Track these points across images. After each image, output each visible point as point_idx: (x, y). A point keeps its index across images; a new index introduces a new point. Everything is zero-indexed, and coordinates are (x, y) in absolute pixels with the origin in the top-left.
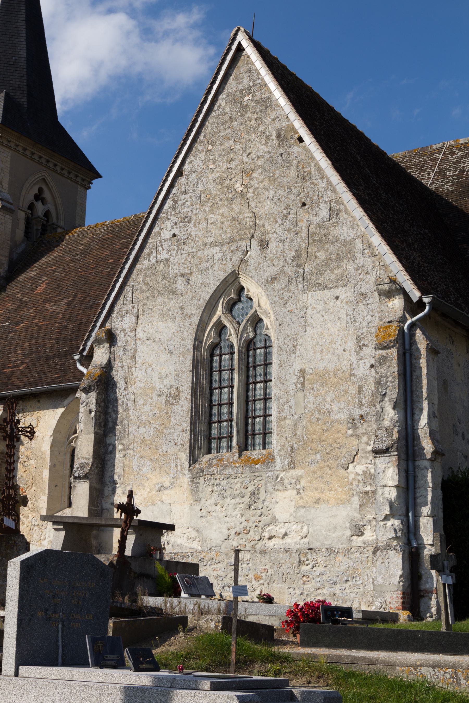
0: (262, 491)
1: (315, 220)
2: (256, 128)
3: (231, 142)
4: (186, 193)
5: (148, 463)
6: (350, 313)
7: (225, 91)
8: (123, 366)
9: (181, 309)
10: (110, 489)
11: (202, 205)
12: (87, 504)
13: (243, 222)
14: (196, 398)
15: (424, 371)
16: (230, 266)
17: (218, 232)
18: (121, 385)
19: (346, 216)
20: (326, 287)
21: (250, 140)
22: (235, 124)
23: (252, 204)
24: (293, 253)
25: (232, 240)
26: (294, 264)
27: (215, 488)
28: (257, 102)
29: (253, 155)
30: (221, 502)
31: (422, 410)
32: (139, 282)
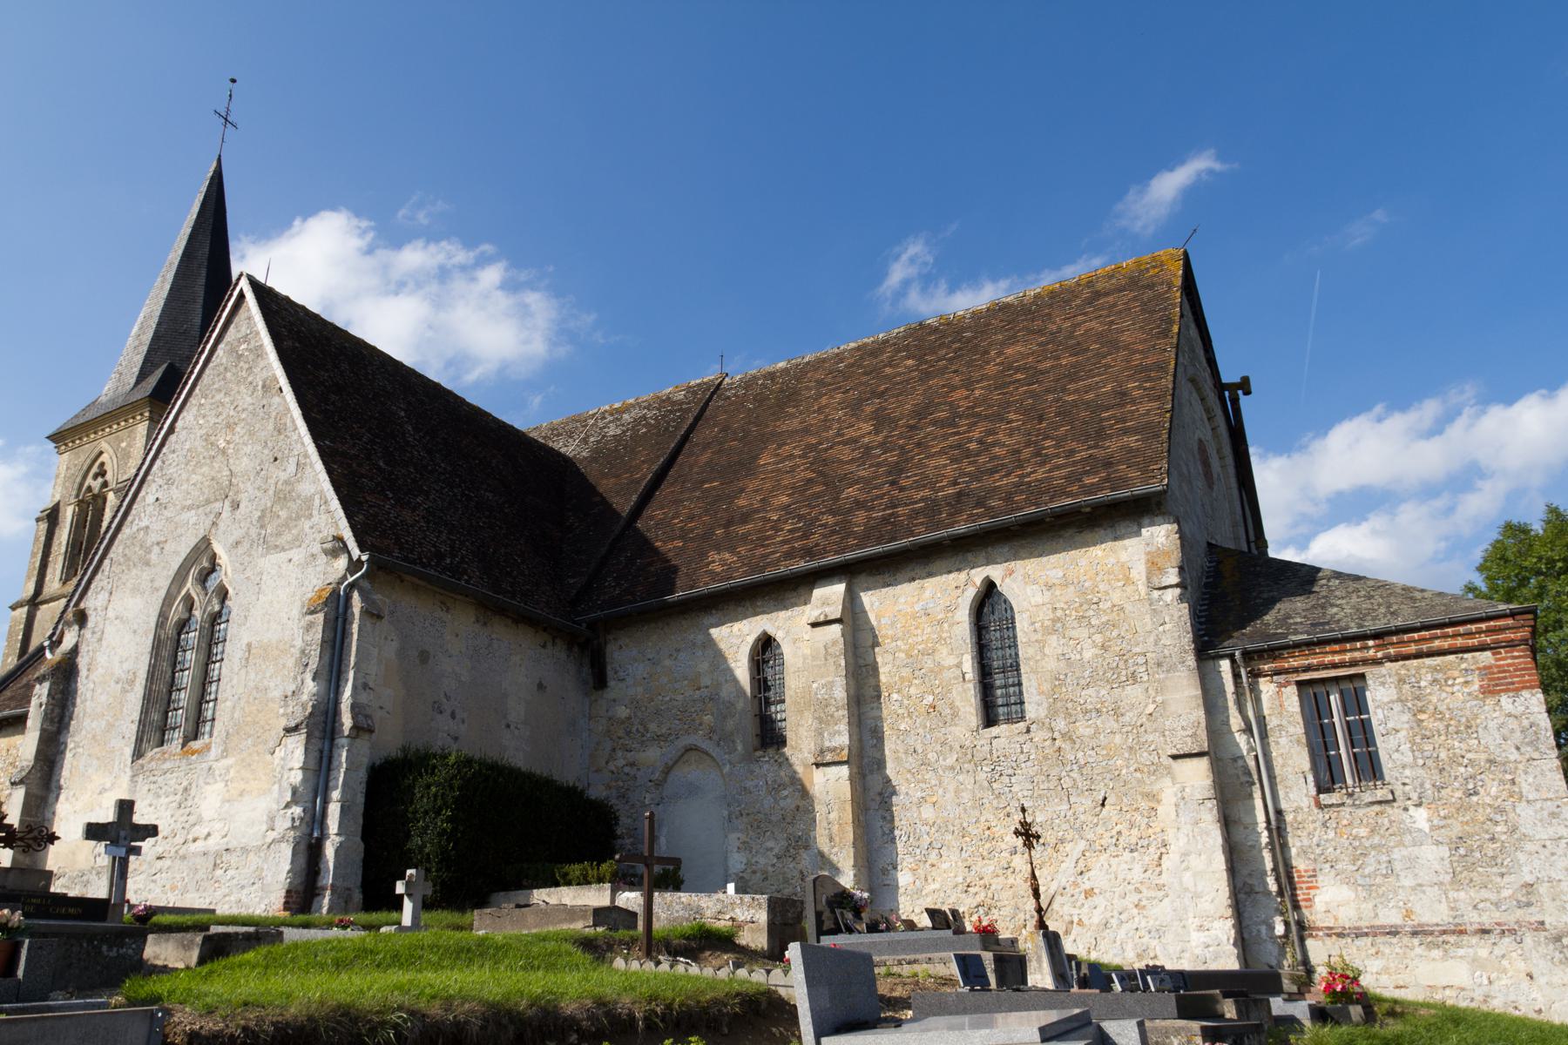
0: (194, 785)
1: (283, 476)
2: (246, 378)
3: (222, 395)
4: (174, 452)
5: (95, 762)
6: (299, 576)
7: (225, 340)
8: (88, 651)
9: (152, 581)
10: (55, 795)
11: (187, 465)
12: (19, 814)
13: (221, 481)
14: (152, 683)
15: (355, 637)
16: (202, 531)
17: (197, 493)
18: (83, 672)
19: (310, 470)
20: (283, 549)
21: (239, 392)
22: (229, 375)
23: (231, 461)
24: (259, 514)
25: (208, 502)
26: (258, 525)
27: (152, 786)
28: (250, 350)
29: (239, 408)
30: (154, 802)
31: (347, 680)
32: (118, 554)
